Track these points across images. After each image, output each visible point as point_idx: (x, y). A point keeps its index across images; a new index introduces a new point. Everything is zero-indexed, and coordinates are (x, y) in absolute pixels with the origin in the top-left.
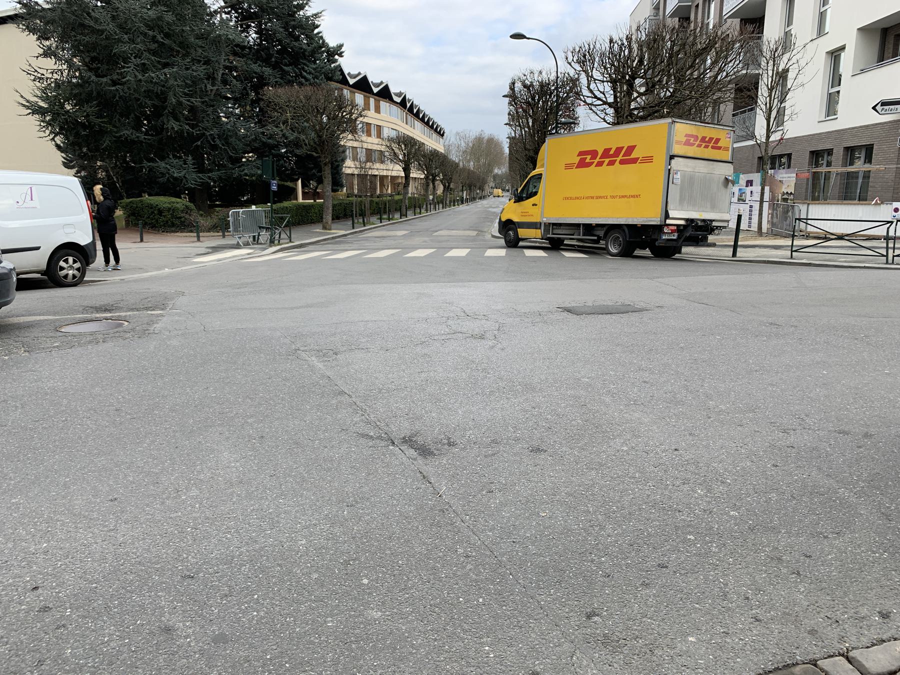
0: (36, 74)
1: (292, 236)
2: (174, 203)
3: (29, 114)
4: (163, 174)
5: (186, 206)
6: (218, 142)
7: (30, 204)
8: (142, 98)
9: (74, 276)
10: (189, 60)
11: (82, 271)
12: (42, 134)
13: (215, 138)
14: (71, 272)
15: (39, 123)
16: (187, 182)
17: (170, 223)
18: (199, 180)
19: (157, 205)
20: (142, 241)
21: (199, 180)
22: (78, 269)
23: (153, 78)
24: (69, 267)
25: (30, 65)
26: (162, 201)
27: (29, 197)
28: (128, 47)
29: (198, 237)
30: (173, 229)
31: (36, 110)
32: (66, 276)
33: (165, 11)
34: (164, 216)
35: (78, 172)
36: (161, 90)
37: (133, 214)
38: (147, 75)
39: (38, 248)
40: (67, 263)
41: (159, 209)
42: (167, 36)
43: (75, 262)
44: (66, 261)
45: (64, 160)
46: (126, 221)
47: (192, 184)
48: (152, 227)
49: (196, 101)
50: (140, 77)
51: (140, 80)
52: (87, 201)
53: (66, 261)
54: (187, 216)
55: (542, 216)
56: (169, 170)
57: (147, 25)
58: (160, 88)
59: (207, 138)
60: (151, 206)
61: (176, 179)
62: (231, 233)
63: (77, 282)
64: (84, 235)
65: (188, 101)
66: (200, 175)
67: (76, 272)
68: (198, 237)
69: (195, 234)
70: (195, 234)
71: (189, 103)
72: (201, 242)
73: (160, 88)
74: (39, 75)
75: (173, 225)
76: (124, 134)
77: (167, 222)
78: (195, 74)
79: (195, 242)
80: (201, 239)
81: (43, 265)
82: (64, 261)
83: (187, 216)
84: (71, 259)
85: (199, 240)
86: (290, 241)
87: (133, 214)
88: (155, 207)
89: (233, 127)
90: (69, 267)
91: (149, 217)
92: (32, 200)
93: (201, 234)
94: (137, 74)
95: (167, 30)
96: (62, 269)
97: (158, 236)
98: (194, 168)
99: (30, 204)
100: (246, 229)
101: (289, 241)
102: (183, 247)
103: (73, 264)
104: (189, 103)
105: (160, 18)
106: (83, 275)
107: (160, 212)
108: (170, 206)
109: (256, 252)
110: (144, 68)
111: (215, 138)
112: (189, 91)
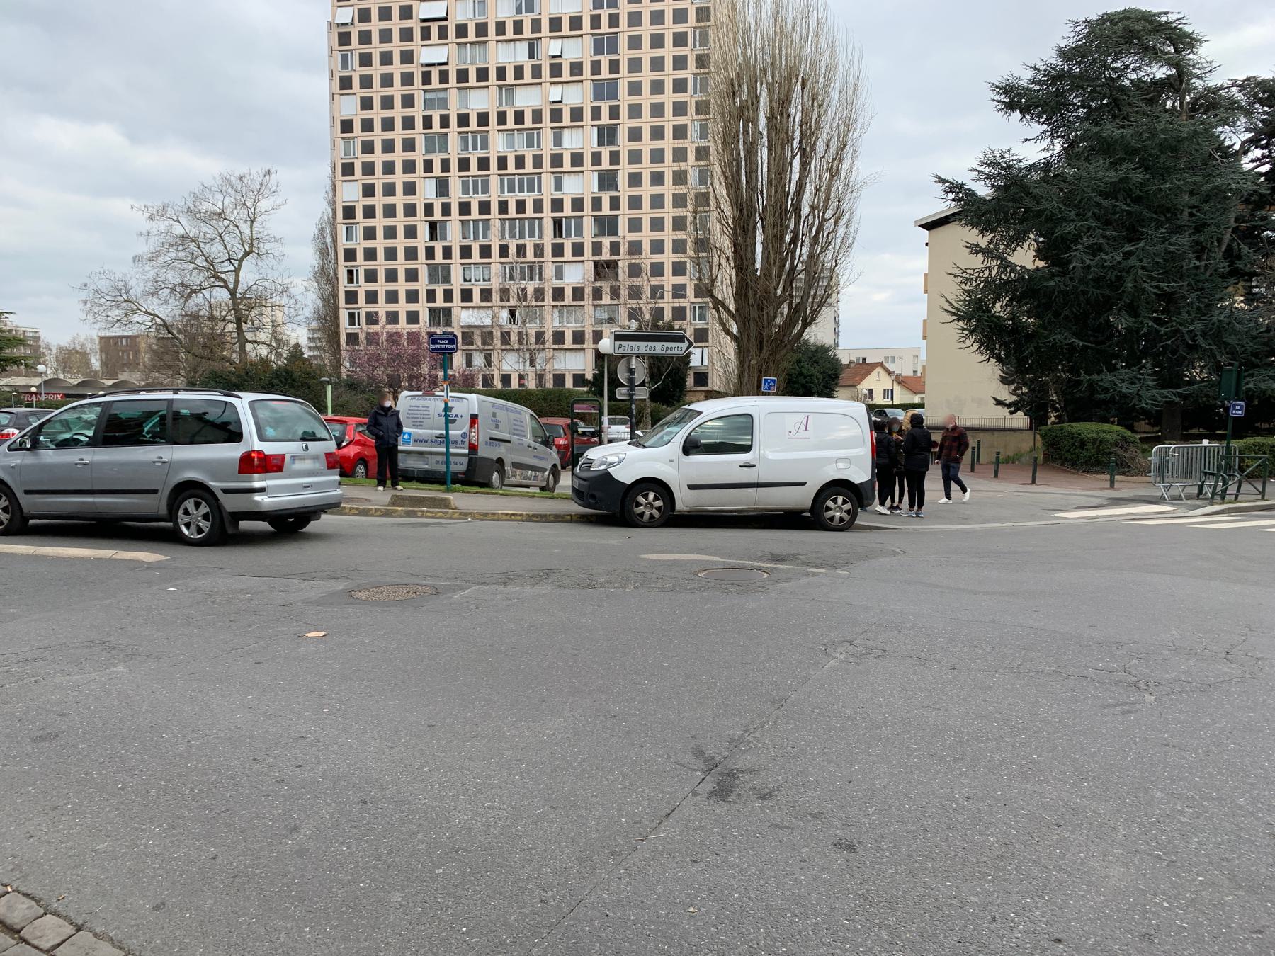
0: (964, 275)
1: (1267, 489)
2: (1104, 432)
3: (954, 321)
4: (1106, 390)
5: (1123, 437)
6: (1200, 341)
7: (803, 433)
8: (1091, 290)
9: (842, 519)
10: (1164, 230)
11: (853, 514)
12: (963, 345)
13: (1196, 336)
14: (838, 514)
15: (961, 331)
16: (1140, 401)
17: (1093, 460)
18: (1160, 399)
19: (1080, 435)
20: (1034, 482)
21: (1160, 399)
22: (848, 512)
23: (1105, 261)
24: (837, 508)
25: (958, 267)
26: (1087, 429)
27: (803, 427)
28: (1073, 227)
29: (1112, 482)
30: (1098, 469)
31: (966, 317)
32: (832, 519)
33: (1133, 169)
34: (1087, 450)
35: (1016, 389)
36: (1117, 276)
37: (1052, 445)
38: (1097, 258)
39: (803, 484)
40: (835, 503)
41: (1081, 440)
42: (1137, 200)
43: (845, 502)
44: (835, 501)
45: (1002, 374)
46: (1044, 454)
47: (1147, 404)
48: (1073, 465)
49: (1168, 286)
50: (1088, 262)
51: (1089, 267)
52: (871, 431)
53: (835, 501)
54: (1121, 452)
55: (942, 491)
56: (1116, 385)
57: (1101, 194)
58: (1115, 273)
59: (1183, 336)
60: (1072, 436)
61: (1124, 396)
62: (1152, 479)
63: (846, 526)
64: (861, 473)
65: (1157, 287)
66: (1164, 392)
67: (844, 515)
68: (1112, 482)
69: (1108, 477)
70: (1108, 477)
71: (1156, 291)
72: (1116, 489)
73: (1115, 273)
74: (968, 276)
75: (1098, 463)
76: (1054, 339)
77: (1090, 457)
78: (1172, 248)
79: (1107, 489)
80: (1116, 485)
81: (808, 503)
82: (832, 500)
83: (1121, 452)
84: (840, 499)
85: (1112, 486)
86: (1263, 499)
87: (1052, 445)
88: (1077, 437)
89: (1229, 317)
90: (837, 508)
91: (1068, 451)
92: (806, 429)
93: (1116, 477)
94: (1084, 257)
95: (1138, 192)
96: (828, 509)
97: (1073, 478)
98: (1154, 381)
99: (805, 434)
100: (1189, 475)
101: (1260, 497)
102: (1070, 494)
103: (656, 508)
104: (1156, 291)
105: (1125, 180)
106: (854, 518)
107: (1083, 444)
108: (1095, 435)
109: (1179, 510)
110: (1095, 250)
111: (1196, 336)
112: (1159, 274)
